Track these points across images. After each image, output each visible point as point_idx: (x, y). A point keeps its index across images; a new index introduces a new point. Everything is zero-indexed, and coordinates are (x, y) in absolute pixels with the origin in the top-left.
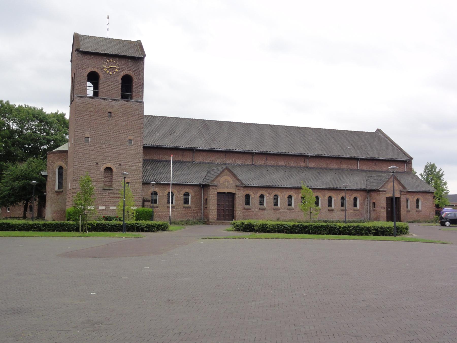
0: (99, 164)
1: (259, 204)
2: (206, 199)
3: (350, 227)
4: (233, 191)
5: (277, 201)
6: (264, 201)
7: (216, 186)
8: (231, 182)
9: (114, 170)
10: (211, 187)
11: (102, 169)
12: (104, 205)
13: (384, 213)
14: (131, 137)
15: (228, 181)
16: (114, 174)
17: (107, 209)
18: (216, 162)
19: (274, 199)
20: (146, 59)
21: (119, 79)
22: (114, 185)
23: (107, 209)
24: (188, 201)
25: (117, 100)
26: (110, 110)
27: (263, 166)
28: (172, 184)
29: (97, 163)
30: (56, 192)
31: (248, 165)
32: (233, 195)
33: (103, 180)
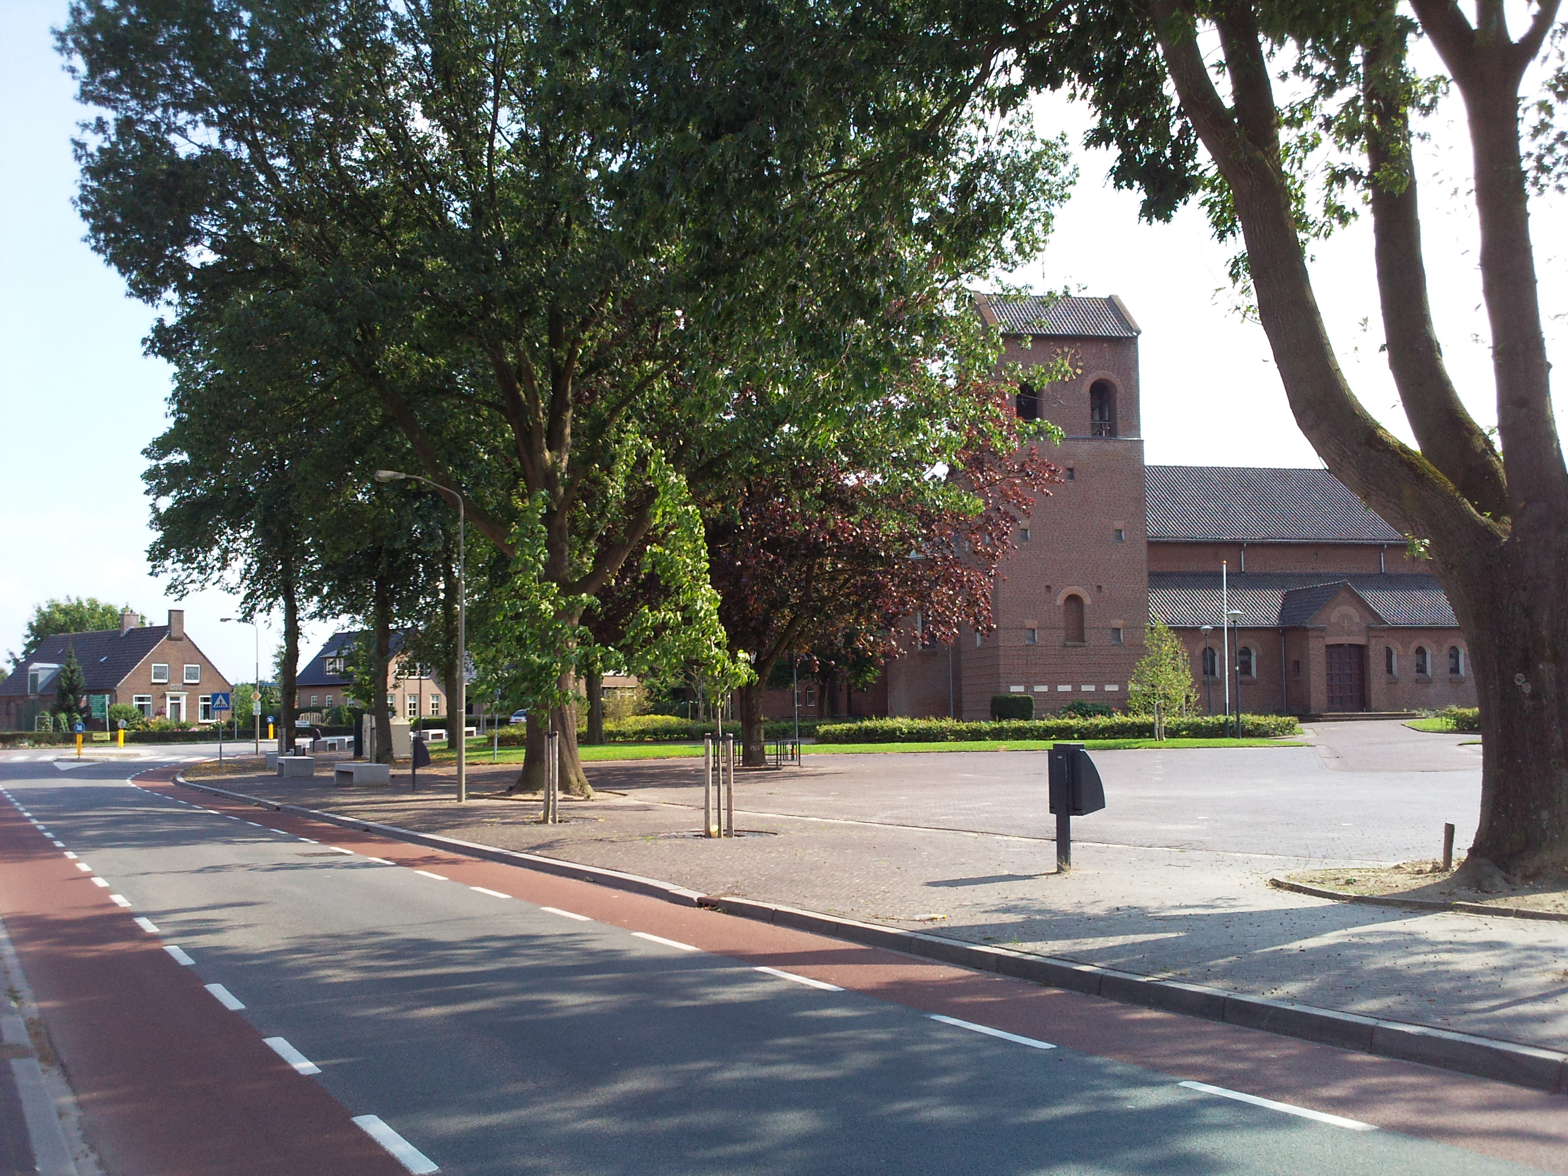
0: (1054, 588)
1: (1415, 669)
2: (1297, 663)
3: (692, 1071)
4: (1360, 640)
5: (1457, 662)
6: (1424, 662)
7: (1323, 630)
8: (1357, 619)
9: (1087, 601)
10: (1310, 634)
11: (1060, 601)
12: (1115, 683)
13: (474, 770)
14: (1119, 524)
15: (1350, 618)
16: (1086, 610)
17: (1076, 690)
18: (1294, 571)
19: (1451, 656)
20: (1141, 340)
21: (1086, 390)
22: (1086, 638)
23: (1076, 690)
24: (1250, 667)
25: (1085, 439)
26: (1070, 463)
27: (1407, 575)
28: (1228, 629)
29: (1048, 587)
30: (920, 654)
31: (1370, 576)
32: (1361, 651)
33: (1063, 624)
